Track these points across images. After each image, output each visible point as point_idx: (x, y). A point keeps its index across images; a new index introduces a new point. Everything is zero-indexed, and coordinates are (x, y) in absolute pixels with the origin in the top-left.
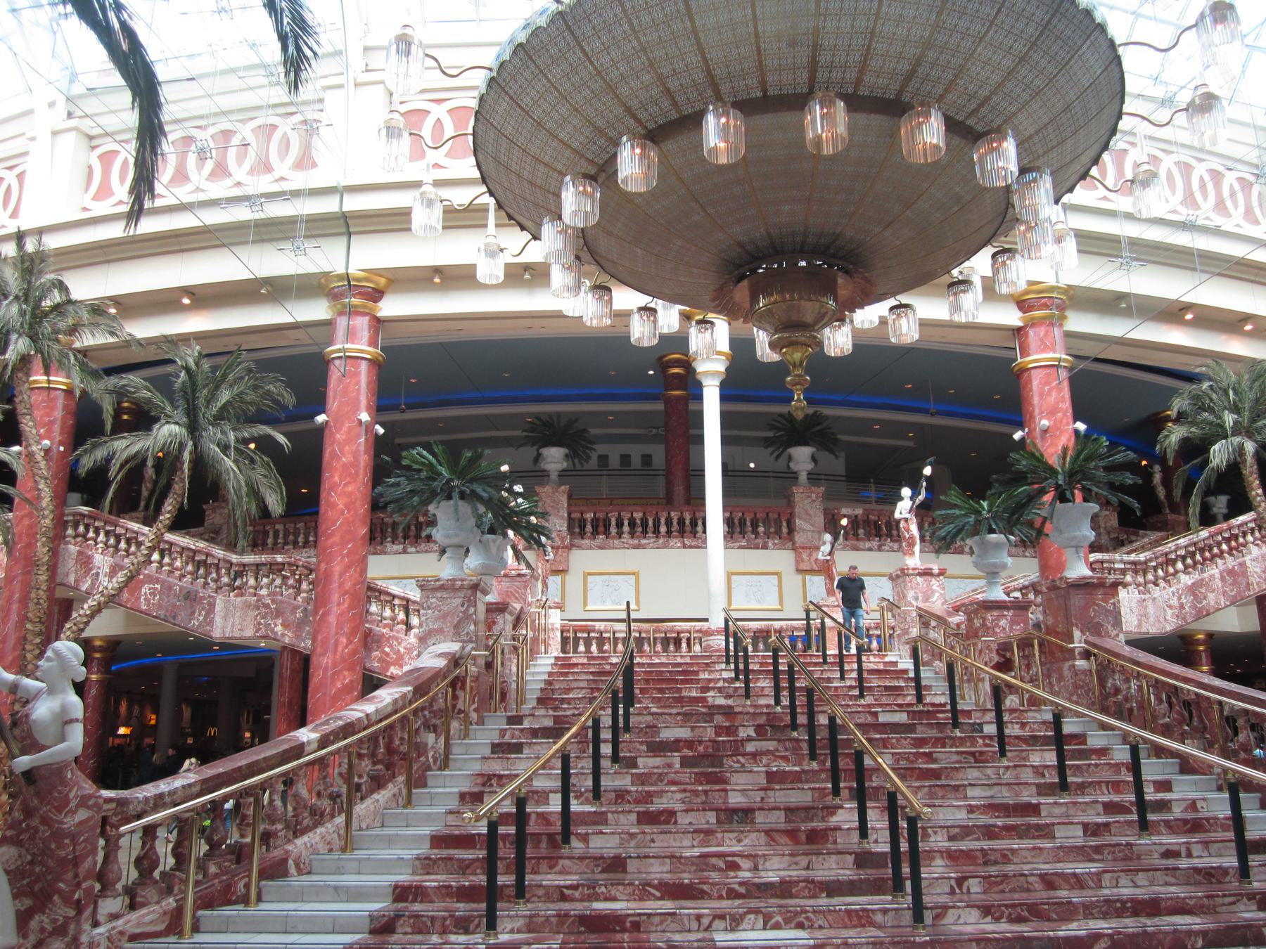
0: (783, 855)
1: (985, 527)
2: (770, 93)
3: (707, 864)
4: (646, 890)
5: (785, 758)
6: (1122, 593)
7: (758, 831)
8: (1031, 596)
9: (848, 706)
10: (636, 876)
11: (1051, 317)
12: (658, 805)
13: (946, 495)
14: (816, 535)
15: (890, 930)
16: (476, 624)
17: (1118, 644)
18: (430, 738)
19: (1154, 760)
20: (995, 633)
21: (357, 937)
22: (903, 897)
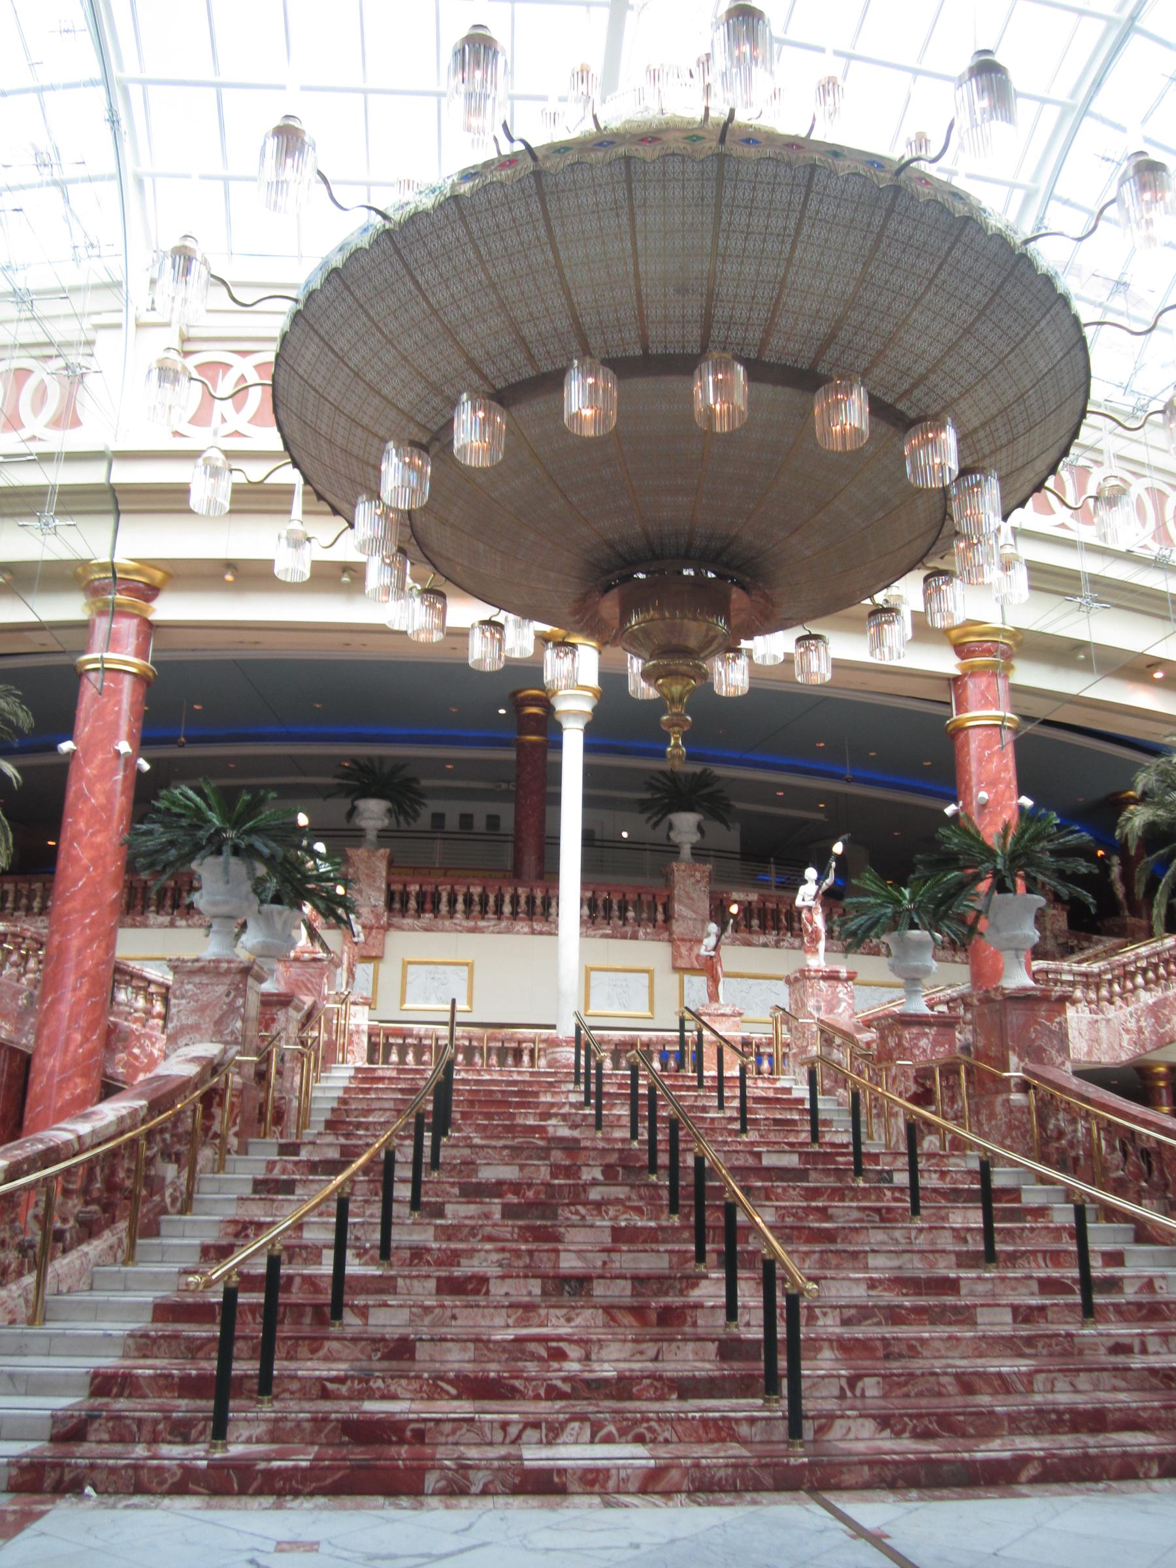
0: (625, 1341)
1: (905, 921)
2: (653, 350)
3: (523, 1351)
4: (438, 1386)
5: (639, 1210)
6: (1071, 1012)
7: (595, 1307)
8: (961, 1011)
9: (725, 1143)
10: (427, 1365)
11: (995, 665)
12: (465, 1269)
13: (858, 877)
14: (699, 926)
15: (759, 1447)
16: (244, 1020)
17: (1064, 1074)
18: (170, 1171)
19: (1103, 1225)
20: (913, 1057)
21: (30, 1446)
22: (777, 1401)
